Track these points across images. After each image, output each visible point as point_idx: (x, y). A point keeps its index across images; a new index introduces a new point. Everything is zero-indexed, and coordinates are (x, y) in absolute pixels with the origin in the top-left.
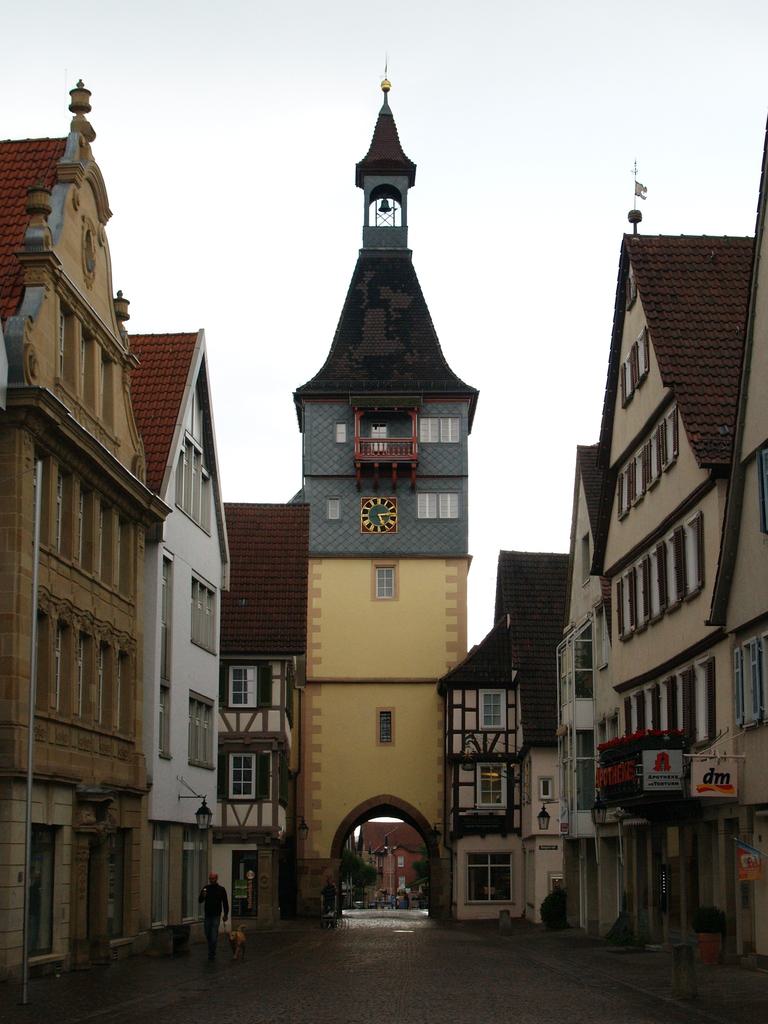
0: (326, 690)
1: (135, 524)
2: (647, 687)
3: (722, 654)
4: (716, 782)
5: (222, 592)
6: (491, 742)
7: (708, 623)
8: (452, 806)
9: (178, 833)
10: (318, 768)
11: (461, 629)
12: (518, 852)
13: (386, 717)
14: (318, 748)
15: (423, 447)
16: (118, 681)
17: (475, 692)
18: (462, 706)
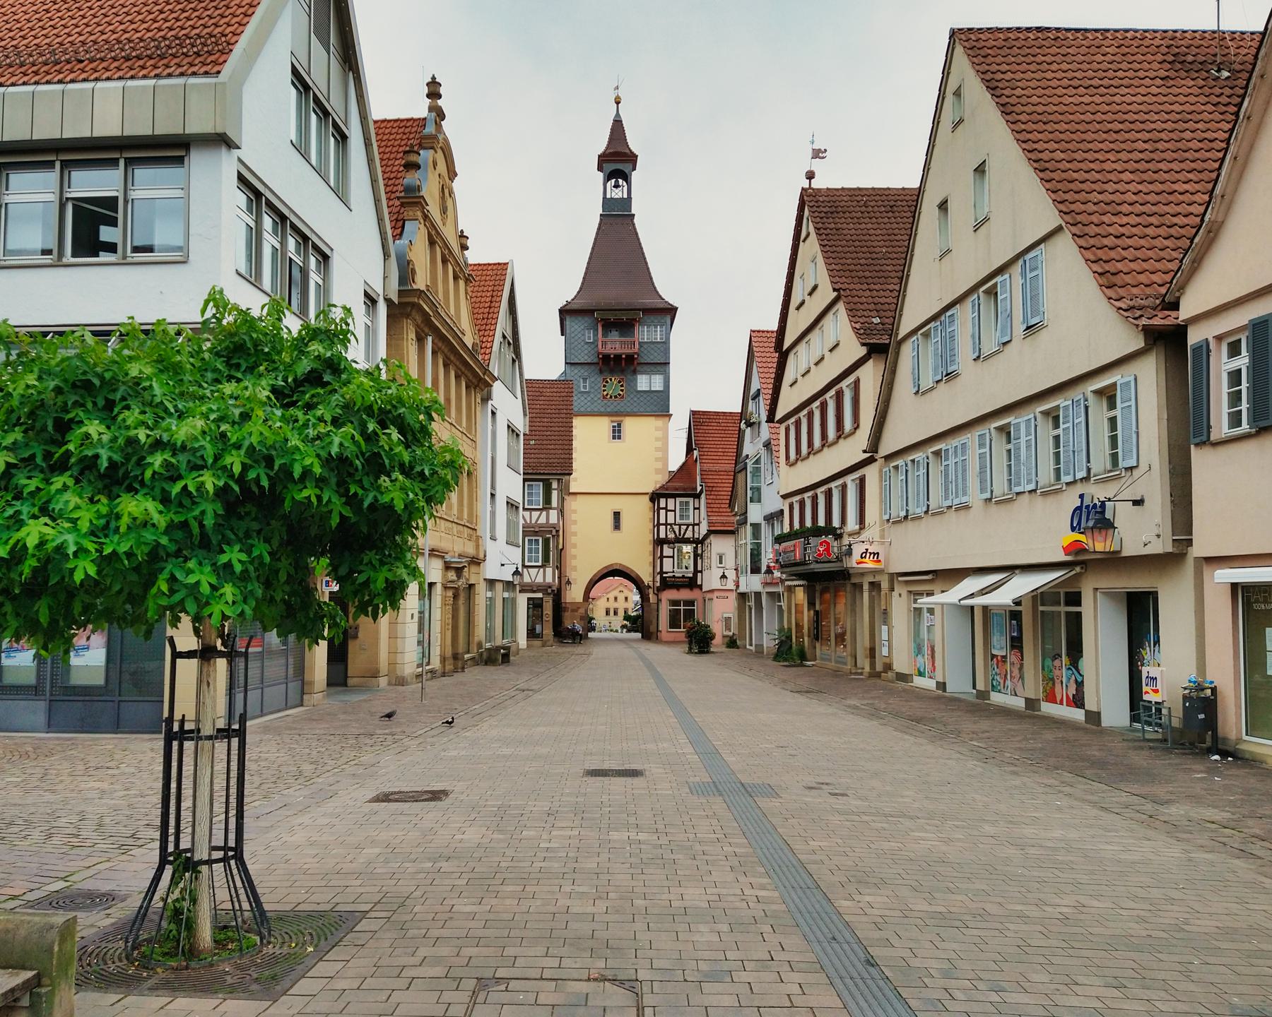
1: (475, 389)
2: (807, 495)
3: (871, 473)
5: (524, 435)
7: (865, 452)
9: (499, 587)
10: (575, 546)
11: (665, 460)
12: (700, 600)
13: (617, 515)
14: (575, 534)
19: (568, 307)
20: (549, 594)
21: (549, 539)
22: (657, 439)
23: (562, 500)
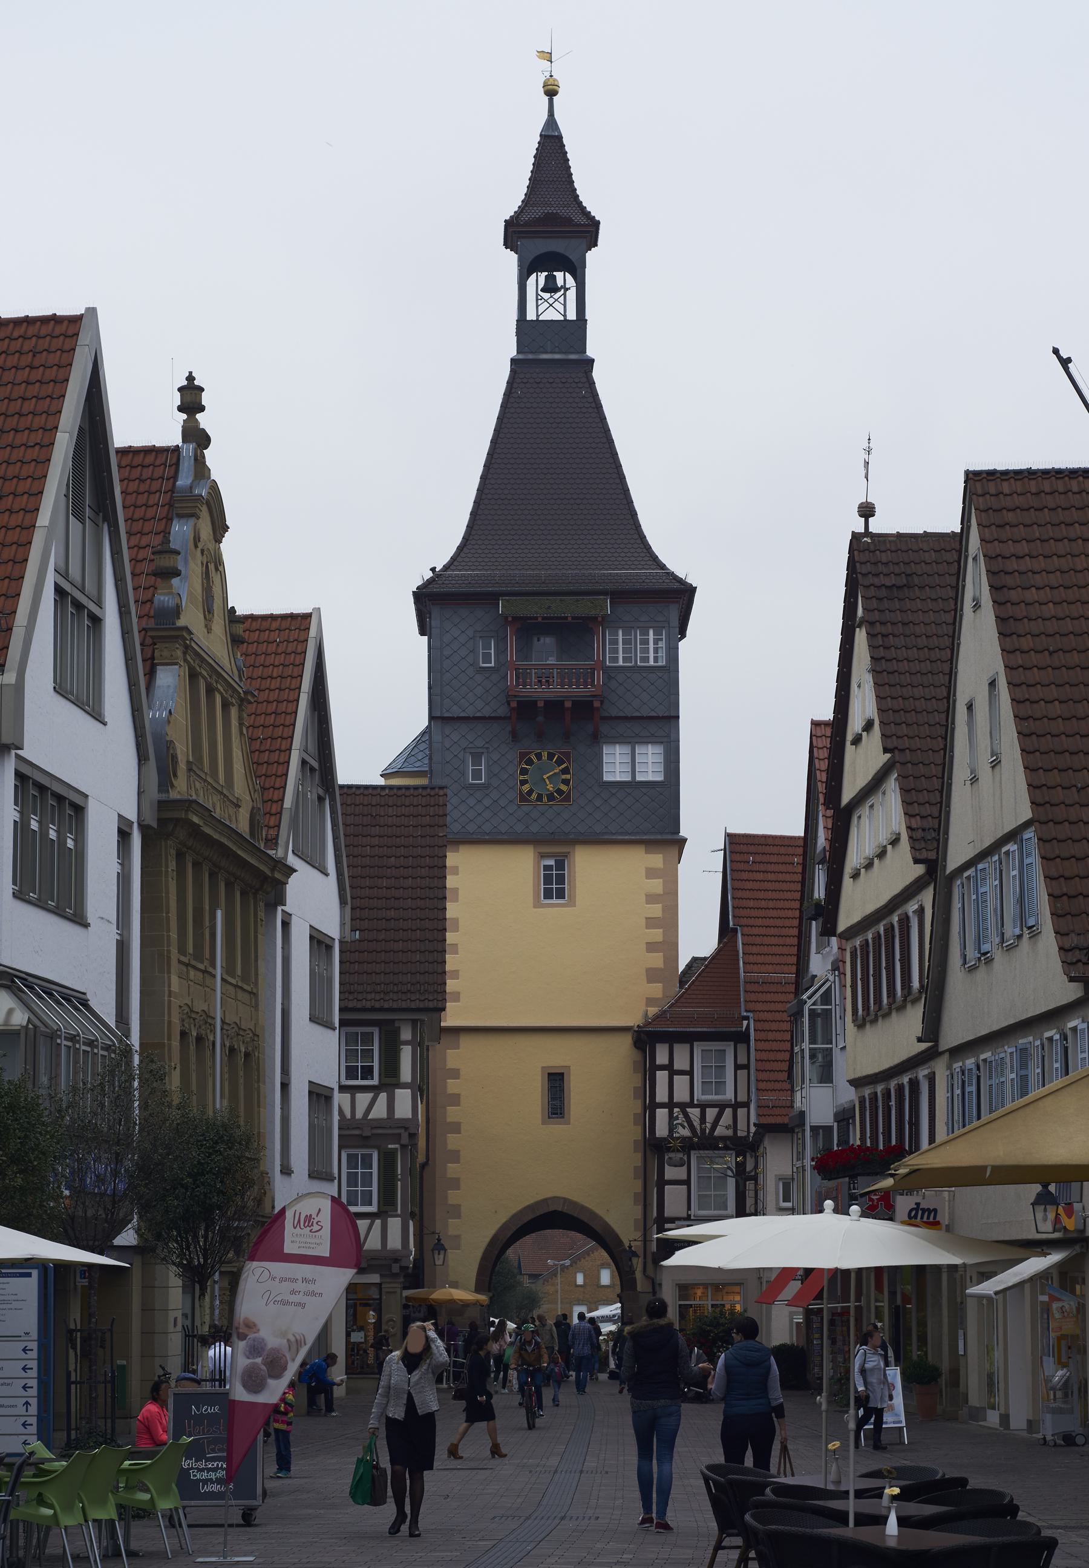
0: (465, 1041)
3: (940, 1068)
4: (922, 1218)
8: (655, 1214)
10: (455, 1157)
11: (670, 946)
13: (556, 1081)
15: (610, 673)
16: (193, 1059)
17: (688, 1046)
18: (669, 1067)
19: (435, 589)
20: (395, 1275)
21: (393, 1152)
22: (651, 899)
23: (422, 1064)
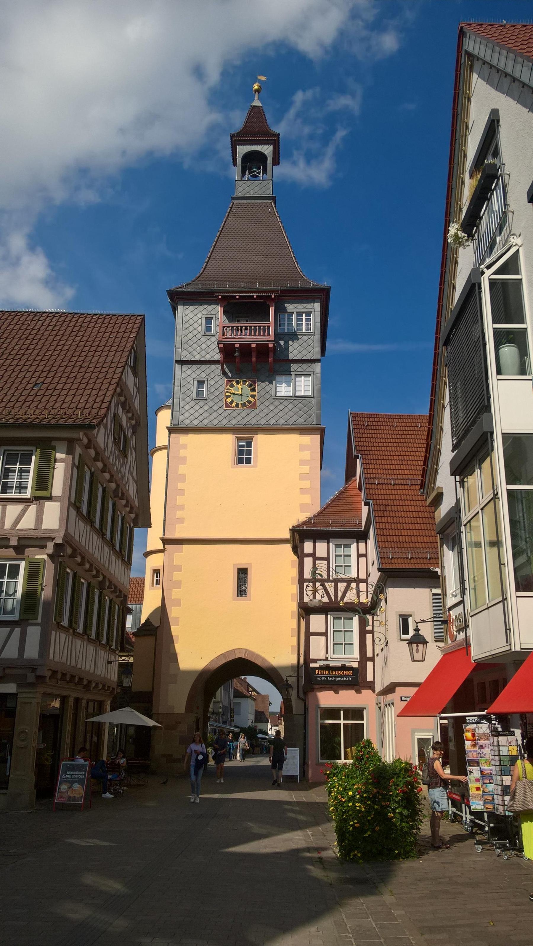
6: (343, 590)
13: (242, 573)
